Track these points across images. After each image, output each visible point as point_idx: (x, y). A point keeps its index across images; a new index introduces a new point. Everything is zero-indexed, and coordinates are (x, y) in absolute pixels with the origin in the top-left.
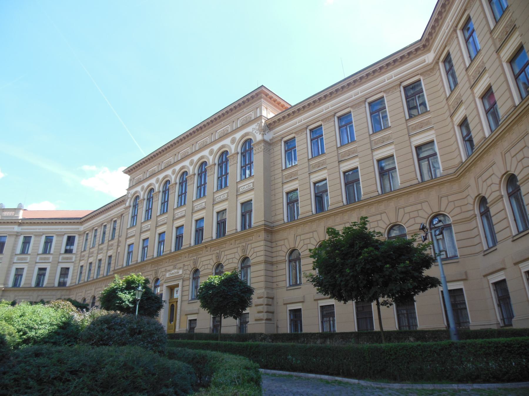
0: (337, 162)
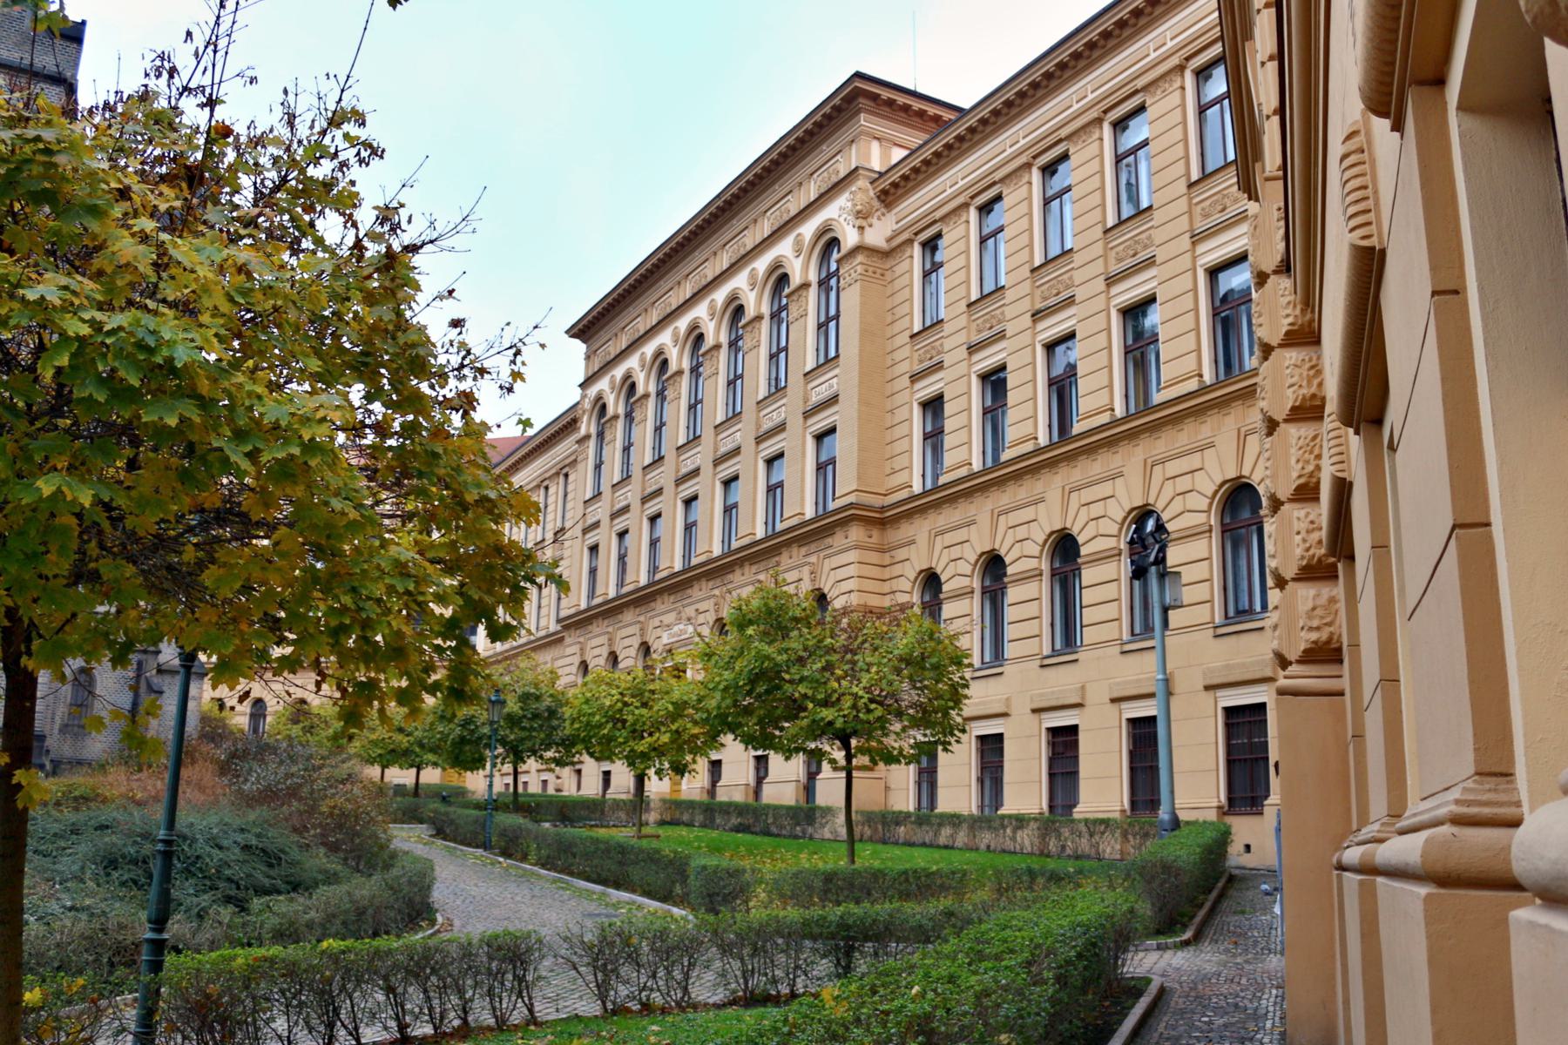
0: (1188, 235)
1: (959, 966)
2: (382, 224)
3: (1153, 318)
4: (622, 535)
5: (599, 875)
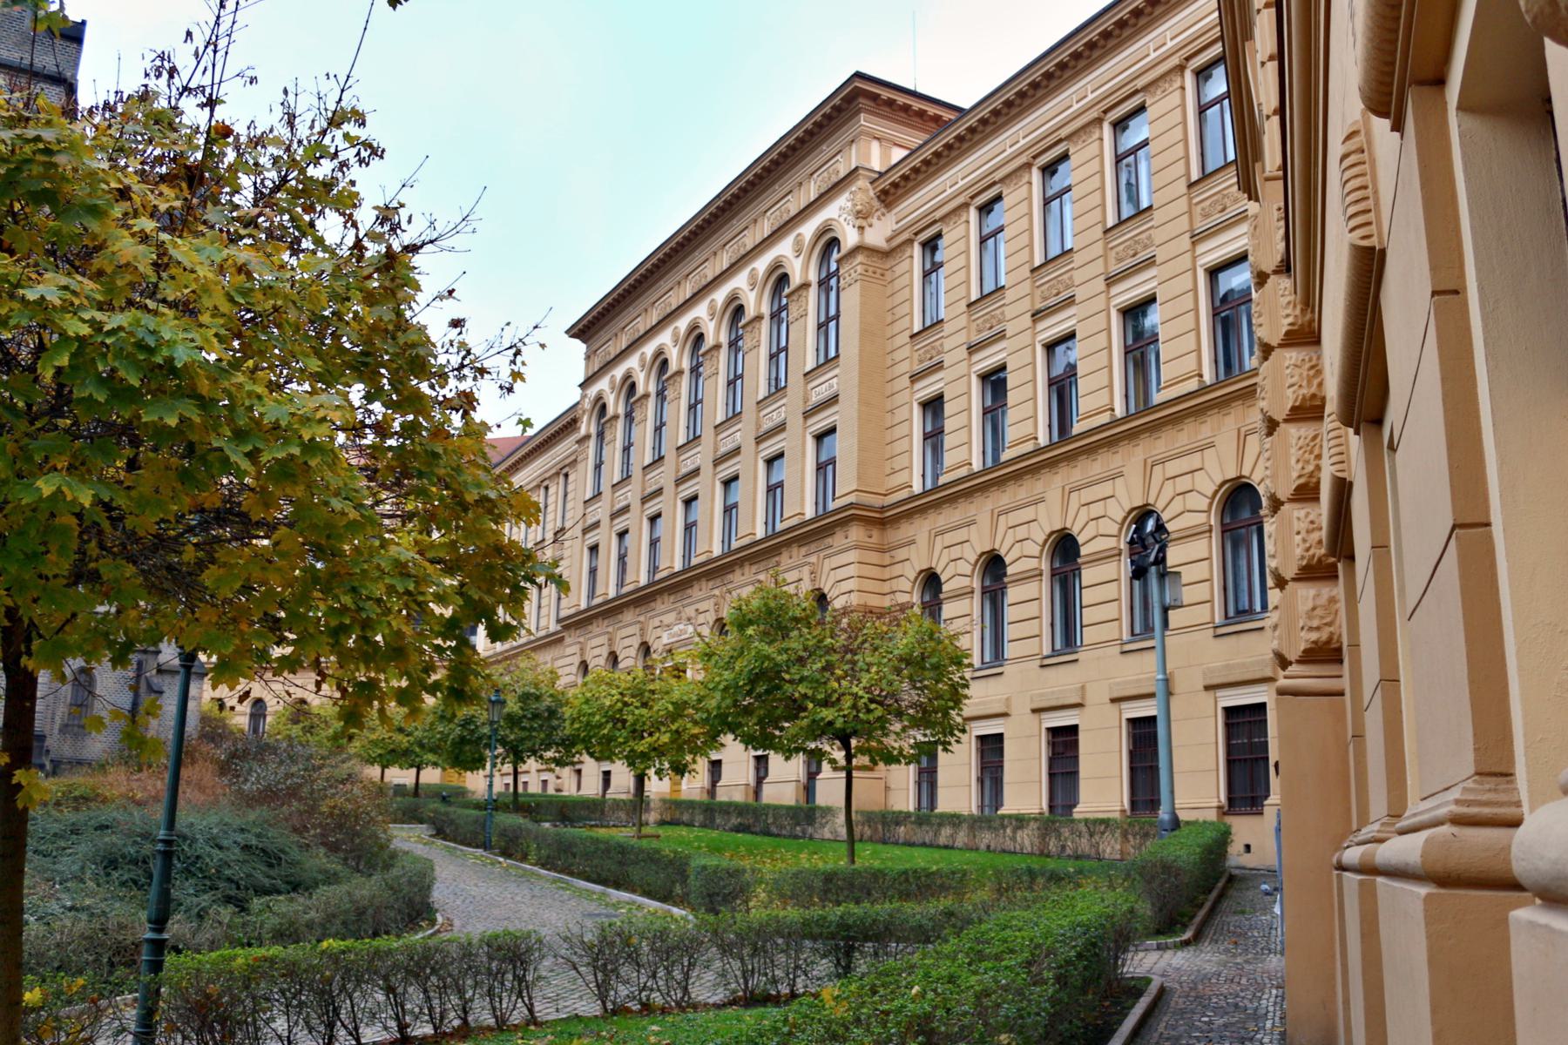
0: (1188, 235)
1: (959, 966)
2: (382, 224)
3: (1153, 318)
4: (622, 535)
5: (599, 875)
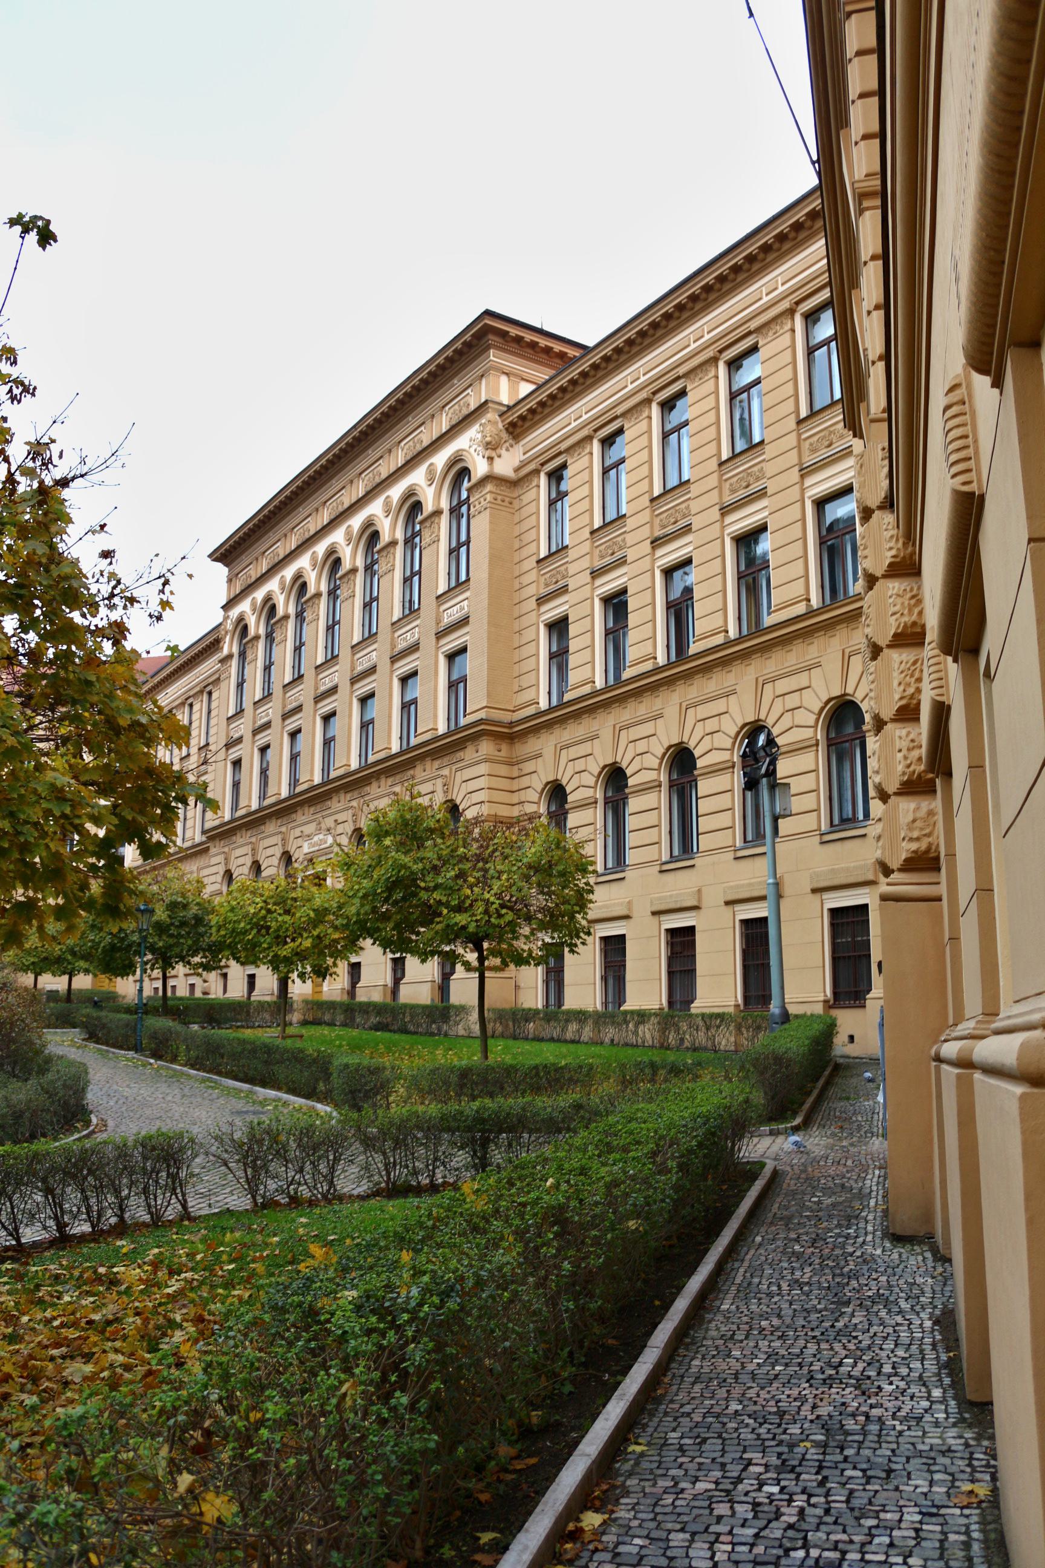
0: (797, 468)
1: (590, 1158)
2: (34, 459)
3: (764, 545)
4: (264, 750)
5: (246, 1074)
